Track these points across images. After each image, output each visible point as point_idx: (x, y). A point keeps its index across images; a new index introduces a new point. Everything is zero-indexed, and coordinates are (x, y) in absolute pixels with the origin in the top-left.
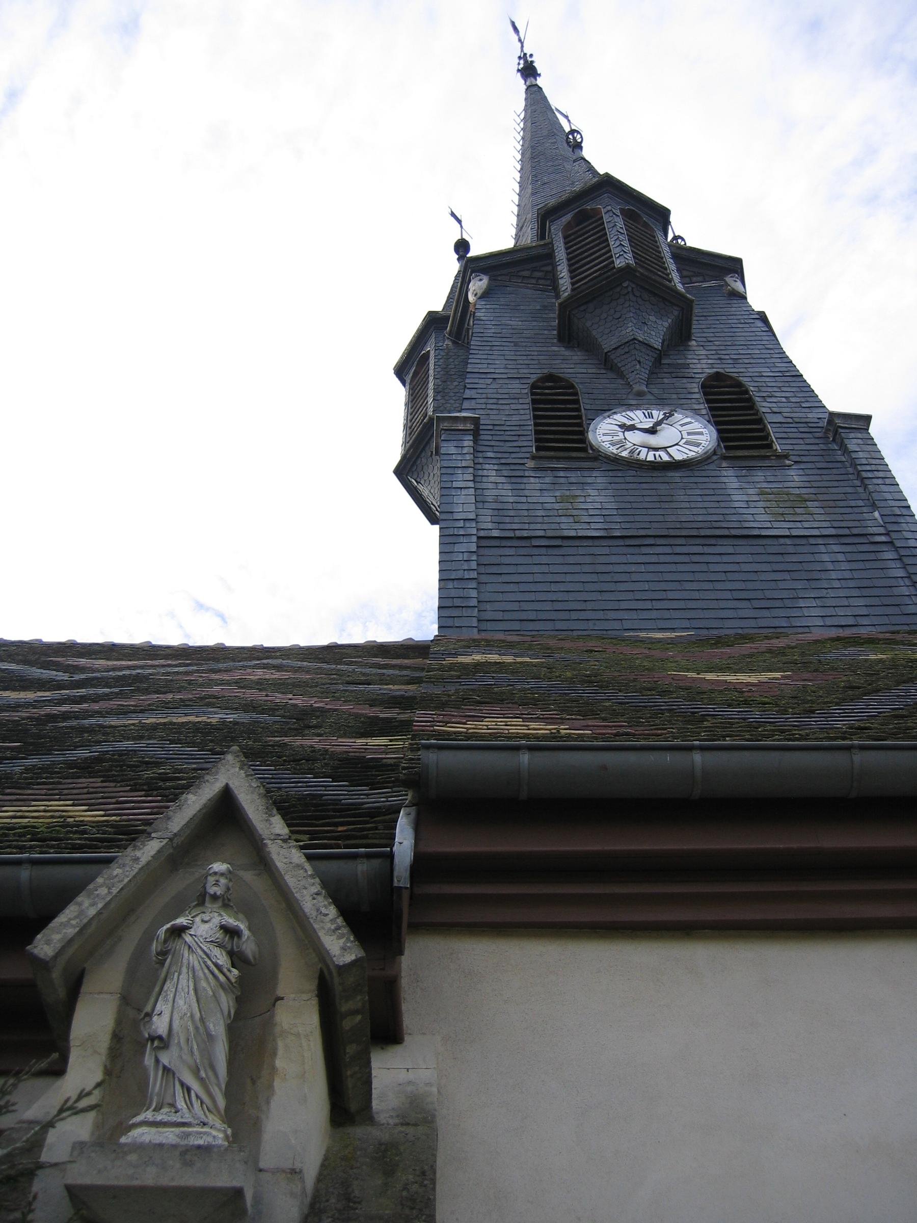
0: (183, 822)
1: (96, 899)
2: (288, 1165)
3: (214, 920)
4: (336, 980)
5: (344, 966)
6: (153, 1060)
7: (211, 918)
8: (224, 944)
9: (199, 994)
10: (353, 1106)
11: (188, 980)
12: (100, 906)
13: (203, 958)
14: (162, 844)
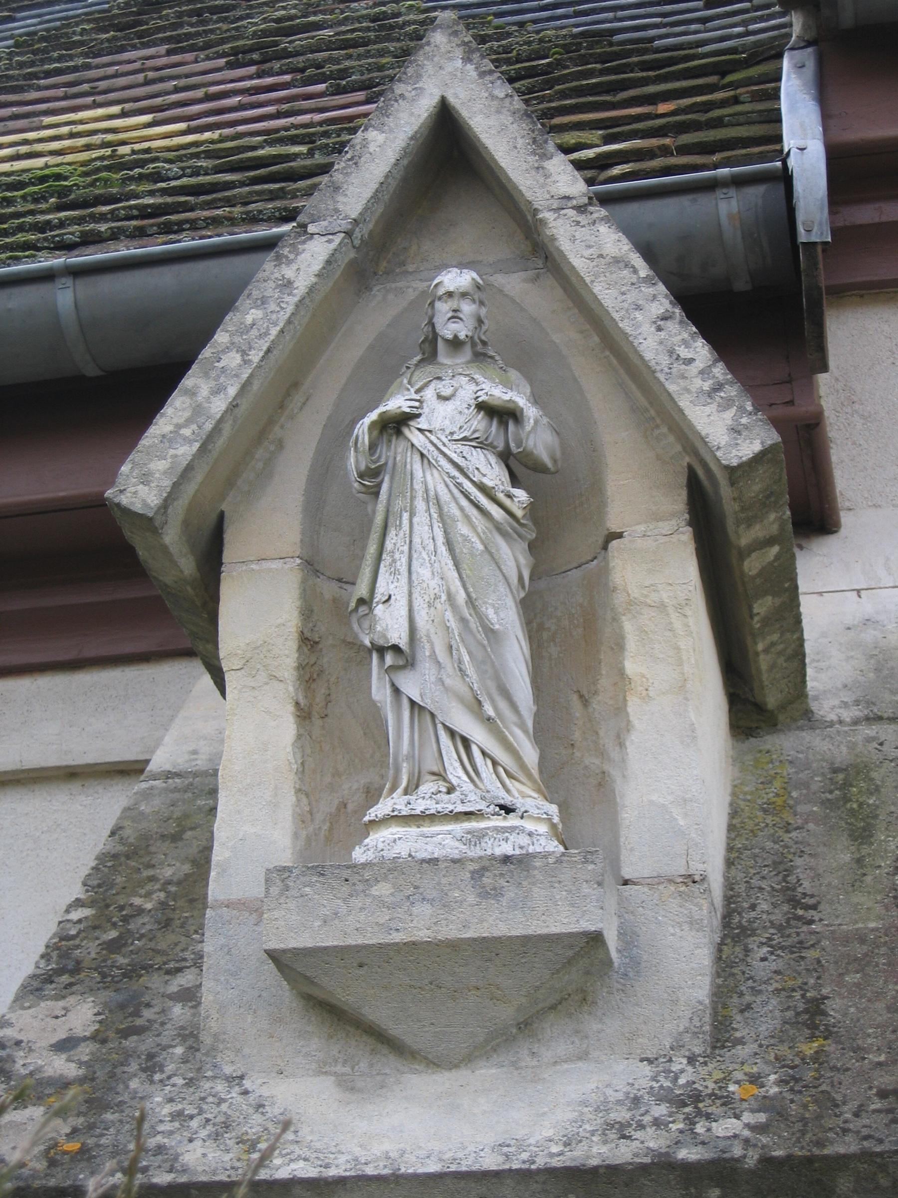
0: (368, 193)
1: (222, 379)
2: (680, 869)
3: (461, 393)
4: (726, 491)
5: (741, 466)
6: (388, 690)
7: (456, 390)
8: (490, 440)
9: (457, 551)
10: (772, 700)
11: (432, 526)
12: (232, 391)
13: (453, 478)
14: (333, 246)
